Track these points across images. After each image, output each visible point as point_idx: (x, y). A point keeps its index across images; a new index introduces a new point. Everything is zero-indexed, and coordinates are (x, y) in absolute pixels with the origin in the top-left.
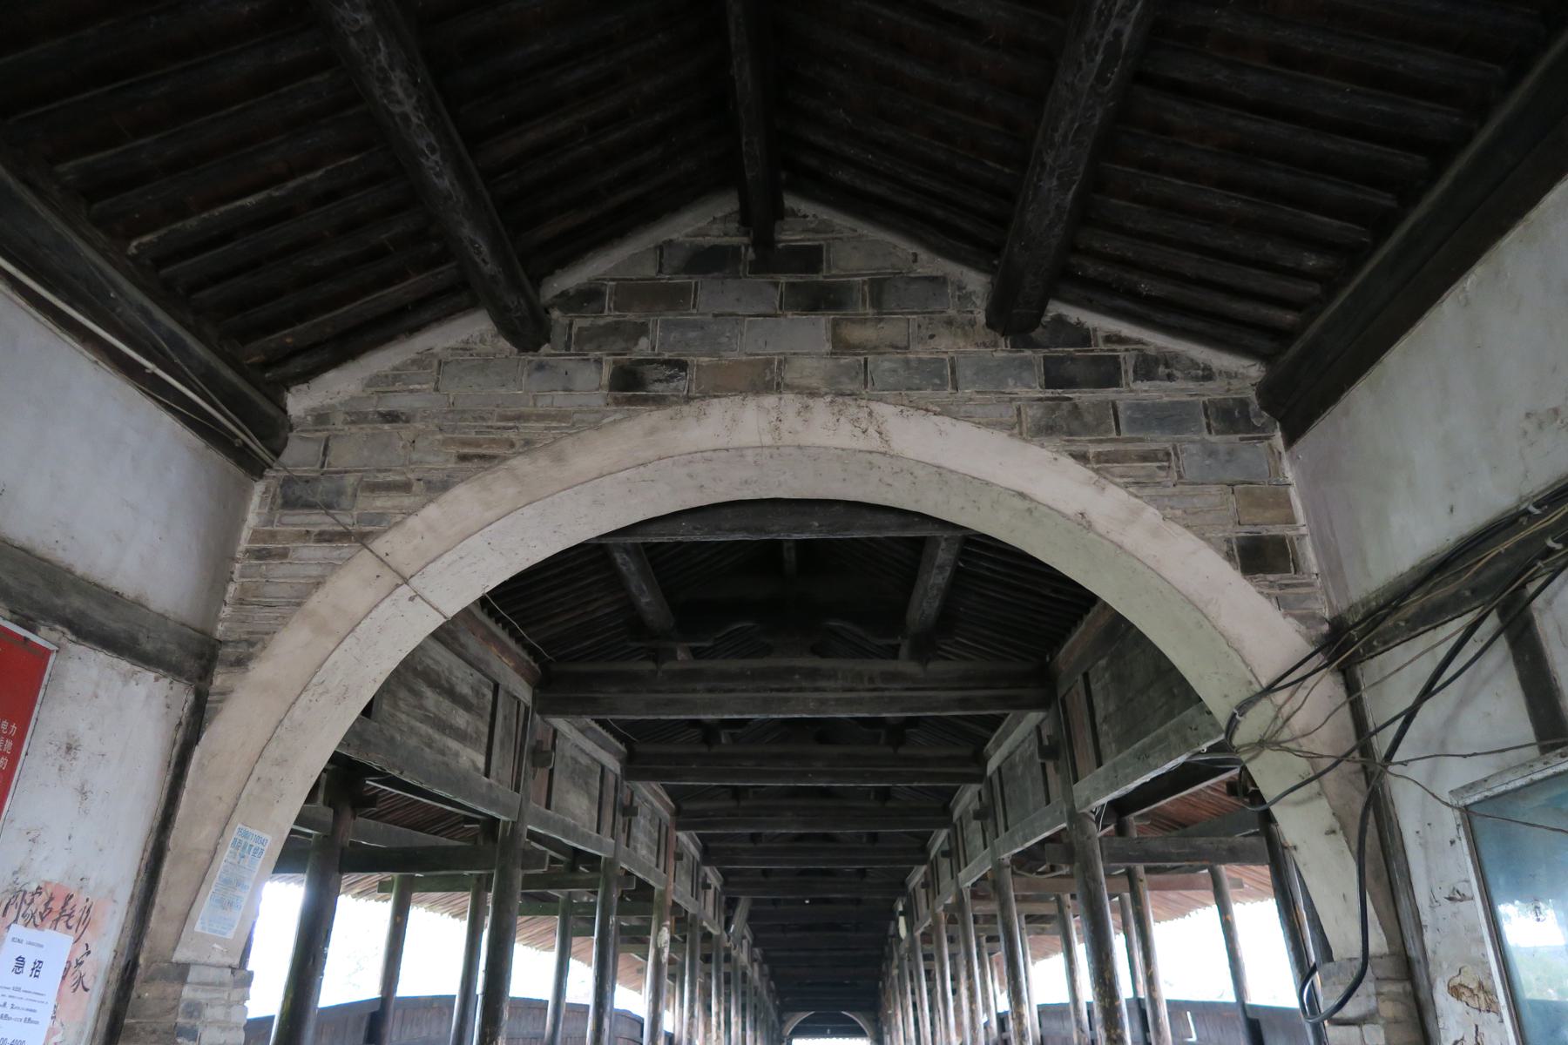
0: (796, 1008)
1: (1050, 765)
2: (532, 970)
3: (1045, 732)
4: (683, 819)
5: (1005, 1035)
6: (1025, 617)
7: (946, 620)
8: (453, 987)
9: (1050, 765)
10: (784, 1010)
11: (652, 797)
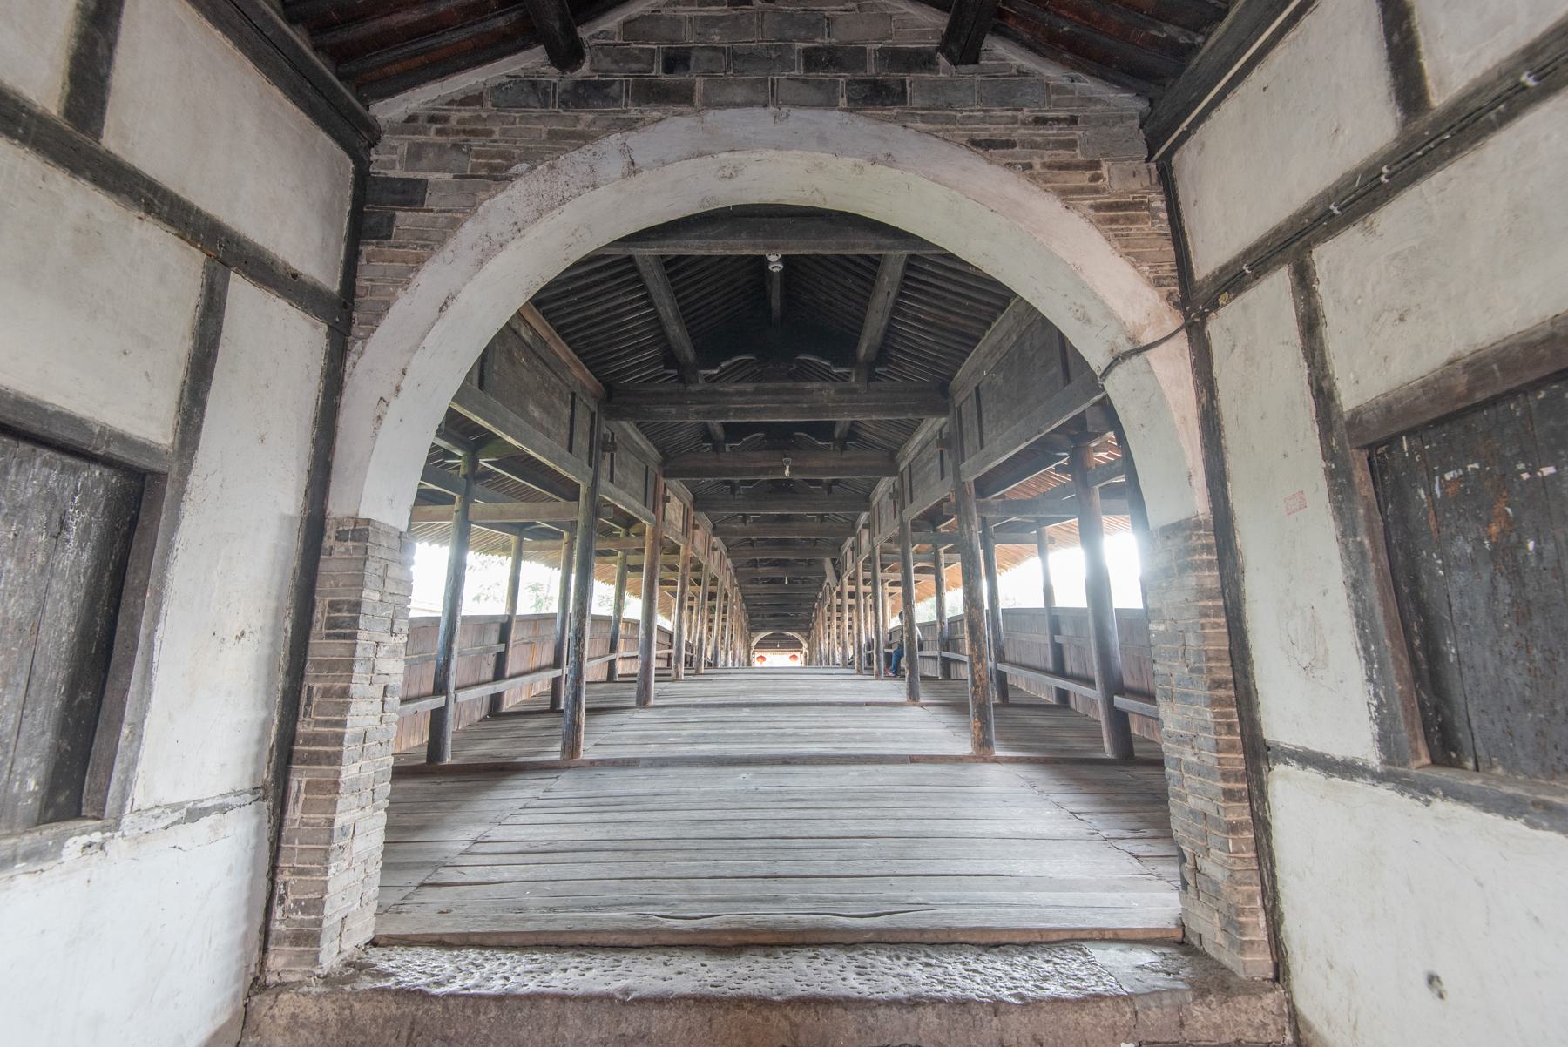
0: (763, 627)
1: (946, 452)
2: (602, 598)
3: (945, 431)
4: (716, 531)
5: (1058, 639)
6: (958, 297)
7: (882, 355)
8: (554, 608)
9: (946, 452)
10: (753, 627)
11: (704, 521)
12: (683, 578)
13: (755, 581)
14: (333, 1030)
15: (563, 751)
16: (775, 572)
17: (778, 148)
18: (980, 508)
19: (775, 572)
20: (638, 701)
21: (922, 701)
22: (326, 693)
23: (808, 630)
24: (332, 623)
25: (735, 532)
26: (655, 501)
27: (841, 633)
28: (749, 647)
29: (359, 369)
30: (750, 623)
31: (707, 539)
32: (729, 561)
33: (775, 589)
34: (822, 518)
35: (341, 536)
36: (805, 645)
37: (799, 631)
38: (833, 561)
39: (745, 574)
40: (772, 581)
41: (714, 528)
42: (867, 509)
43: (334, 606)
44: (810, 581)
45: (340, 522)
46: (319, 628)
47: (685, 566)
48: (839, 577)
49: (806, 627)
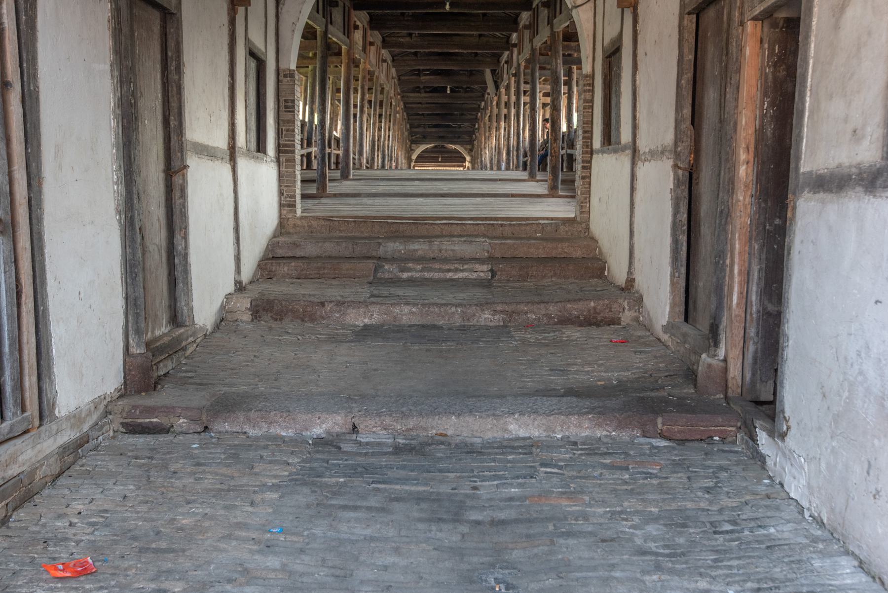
0: (424, 139)
12: (363, 88)
13: (417, 90)
14: (307, 228)
15: (318, 189)
16: (438, 81)
17: (434, 327)
18: (565, 48)
19: (438, 81)
20: (342, 176)
21: (538, 178)
22: (287, 130)
23: (471, 142)
24: (286, 107)
25: (401, 45)
26: (348, 29)
27: (494, 141)
28: (409, 160)
29: (283, 11)
30: (411, 134)
31: (378, 52)
32: (393, 70)
33: (437, 98)
34: (480, 35)
35: (285, 76)
36: (468, 158)
37: (462, 144)
38: (493, 72)
39: (407, 84)
40: (435, 90)
41: (384, 41)
42: (516, 31)
43: (286, 101)
44: (472, 90)
45: (284, 71)
46: (282, 108)
47: (364, 77)
48: (497, 88)
49: (470, 139)
